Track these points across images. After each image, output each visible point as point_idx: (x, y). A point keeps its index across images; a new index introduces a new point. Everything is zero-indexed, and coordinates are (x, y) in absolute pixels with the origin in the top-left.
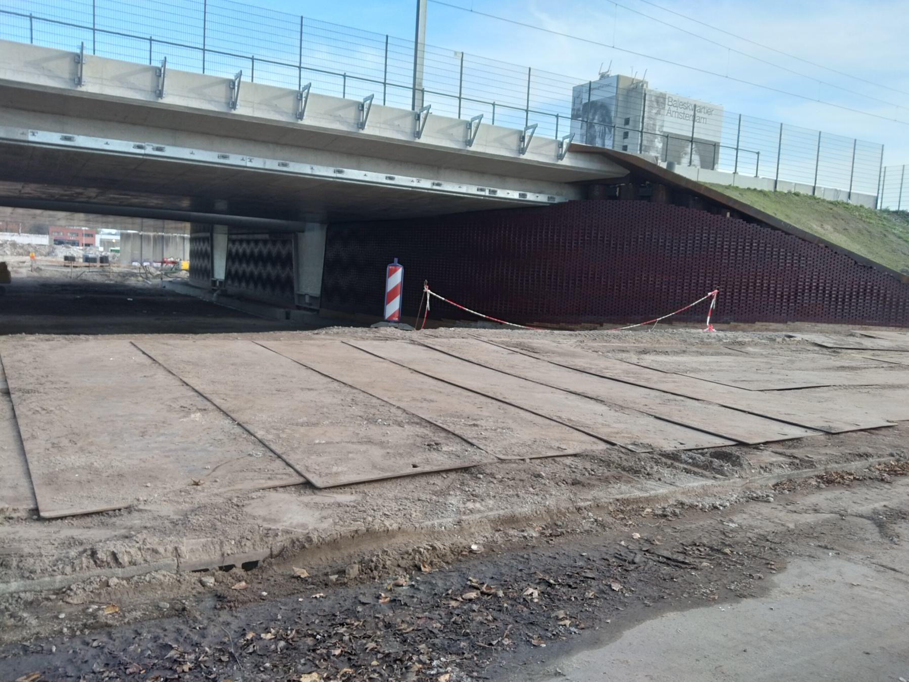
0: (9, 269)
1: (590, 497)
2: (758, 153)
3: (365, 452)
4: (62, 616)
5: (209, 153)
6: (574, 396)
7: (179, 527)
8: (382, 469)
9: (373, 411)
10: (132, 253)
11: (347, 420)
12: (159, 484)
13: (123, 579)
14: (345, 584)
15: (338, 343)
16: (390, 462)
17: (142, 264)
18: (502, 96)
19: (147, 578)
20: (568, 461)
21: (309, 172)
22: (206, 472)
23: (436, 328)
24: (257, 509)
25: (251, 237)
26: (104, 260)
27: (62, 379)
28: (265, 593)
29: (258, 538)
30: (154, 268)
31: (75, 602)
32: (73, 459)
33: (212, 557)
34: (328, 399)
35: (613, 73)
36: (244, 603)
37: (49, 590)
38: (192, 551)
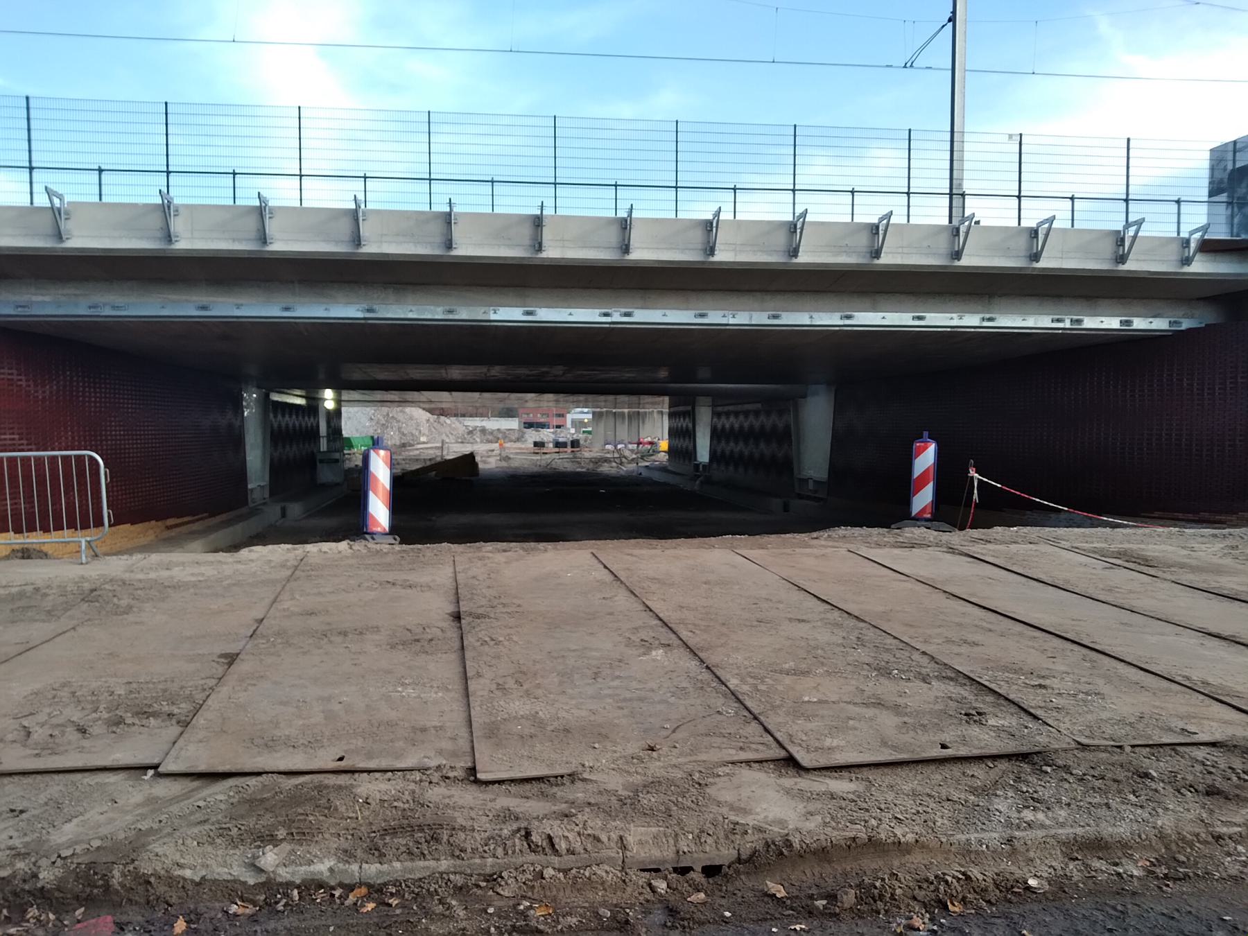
0: (478, 459)
1: (1238, 820)
3: (871, 719)
4: (491, 910)
5: (685, 312)
6: (1216, 642)
7: (627, 808)
8: (895, 748)
9: (886, 657)
11: (849, 668)
12: (609, 745)
13: (559, 871)
14: (836, 915)
15: (843, 551)
16: (907, 738)
19: (587, 874)
20: (1200, 753)
22: (665, 733)
23: (989, 526)
24: (722, 791)
25: (739, 408)
26: (575, 444)
27: (515, 601)
28: (728, 914)
29: (722, 835)
30: (629, 450)
31: (506, 894)
32: (518, 706)
33: (663, 853)
34: (823, 636)
36: (701, 923)
37: (479, 875)
38: (640, 843)
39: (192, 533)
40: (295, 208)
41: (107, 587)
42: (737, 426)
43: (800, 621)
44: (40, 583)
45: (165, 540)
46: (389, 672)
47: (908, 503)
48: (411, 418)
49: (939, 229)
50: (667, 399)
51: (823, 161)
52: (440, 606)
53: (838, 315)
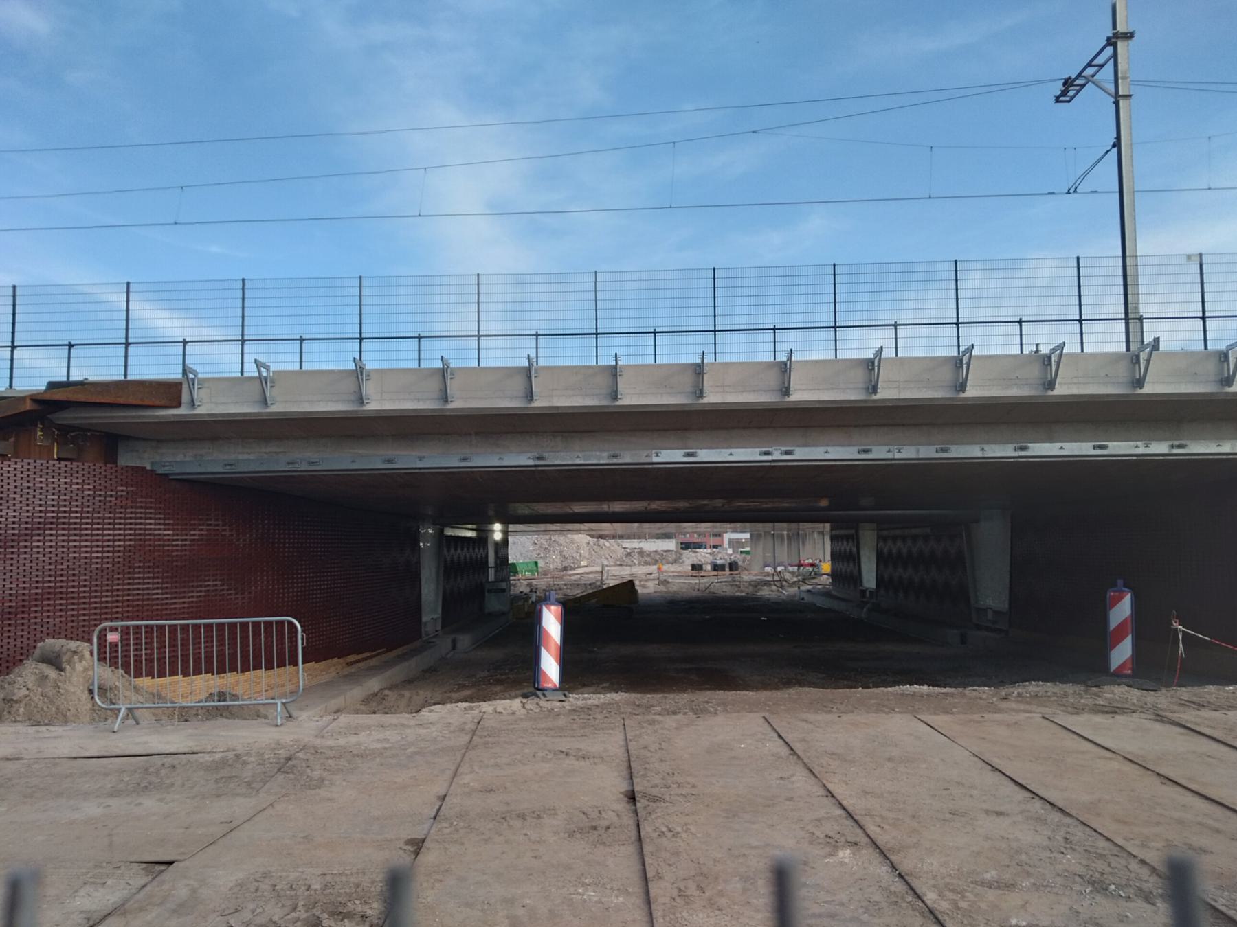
0: (637, 583)
9: (1100, 865)
10: (764, 557)
11: (1059, 880)
15: (1037, 718)
17: (775, 569)
21: (979, 454)
26: (733, 566)
27: (689, 779)
30: (789, 572)
34: (1026, 835)
39: (370, 669)
40: (474, 368)
41: (301, 755)
42: (905, 551)
43: (1000, 814)
44: (240, 750)
45: (345, 676)
46: (568, 867)
47: (1106, 659)
48: (572, 542)
49: (1114, 358)
50: (828, 526)
51: (978, 275)
52: (612, 784)
53: (1011, 446)
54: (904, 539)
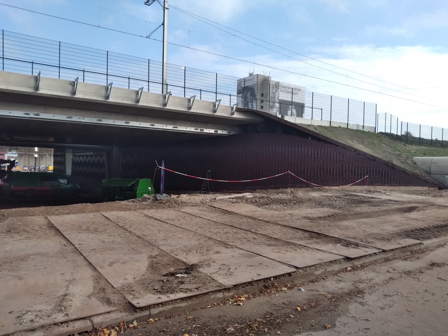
2: (322, 109)
18: (203, 79)
21: (113, 124)
35: (255, 73)
50: (53, 149)
54: (83, 156)
